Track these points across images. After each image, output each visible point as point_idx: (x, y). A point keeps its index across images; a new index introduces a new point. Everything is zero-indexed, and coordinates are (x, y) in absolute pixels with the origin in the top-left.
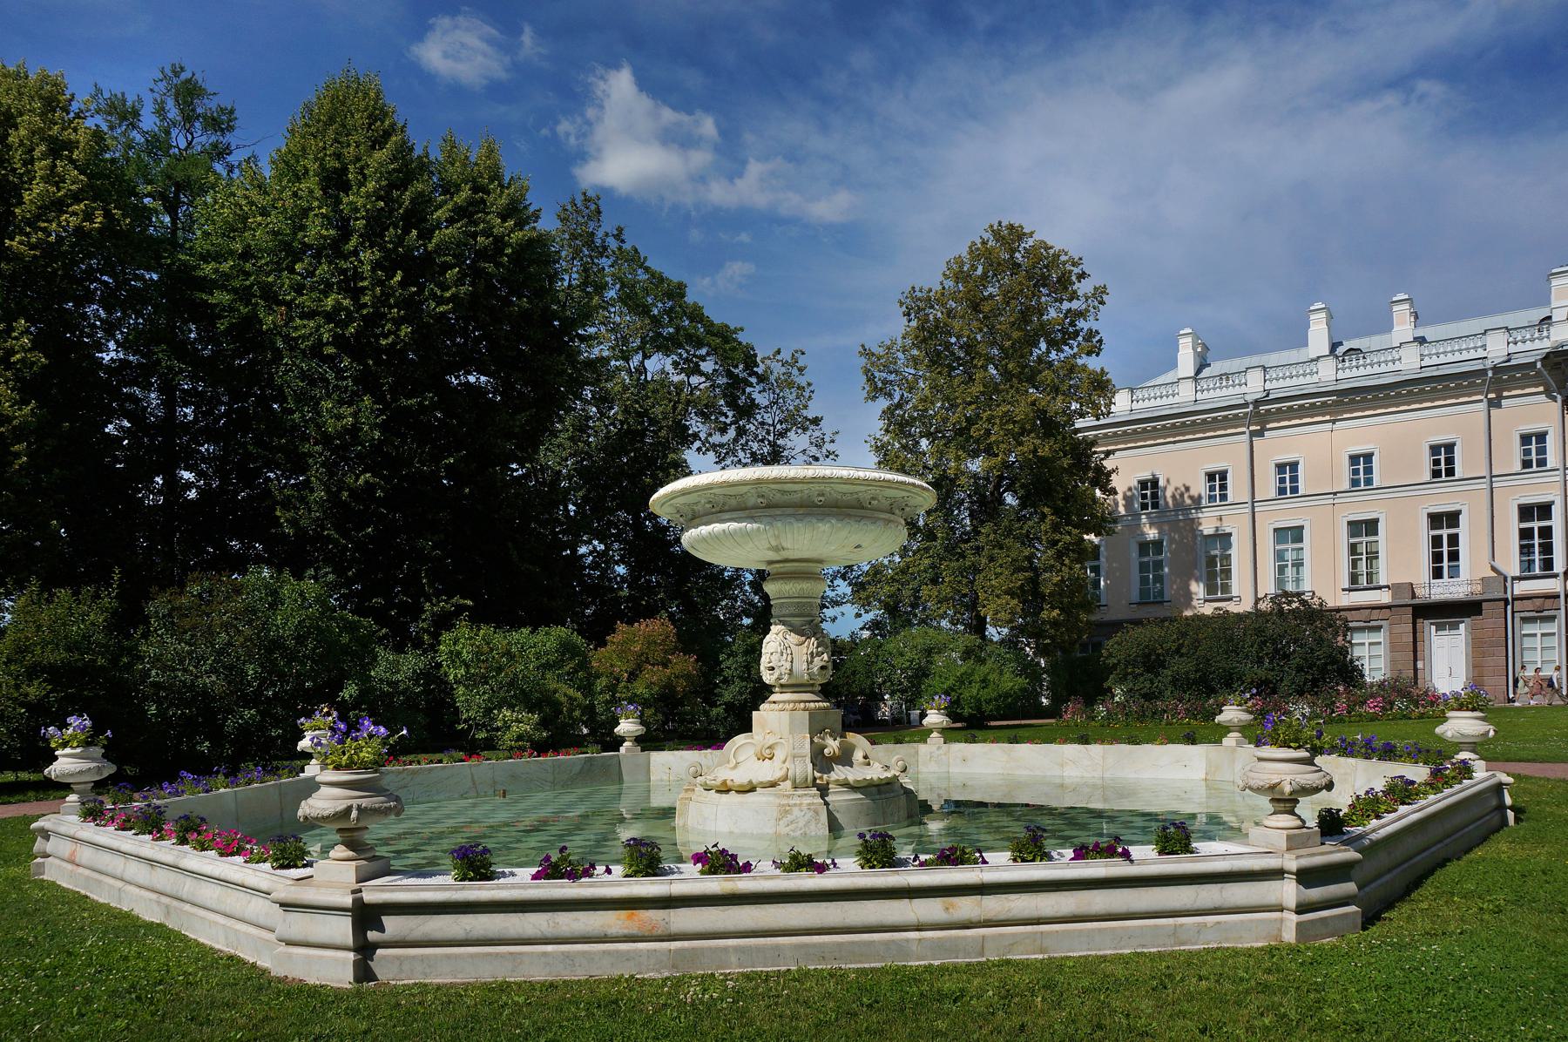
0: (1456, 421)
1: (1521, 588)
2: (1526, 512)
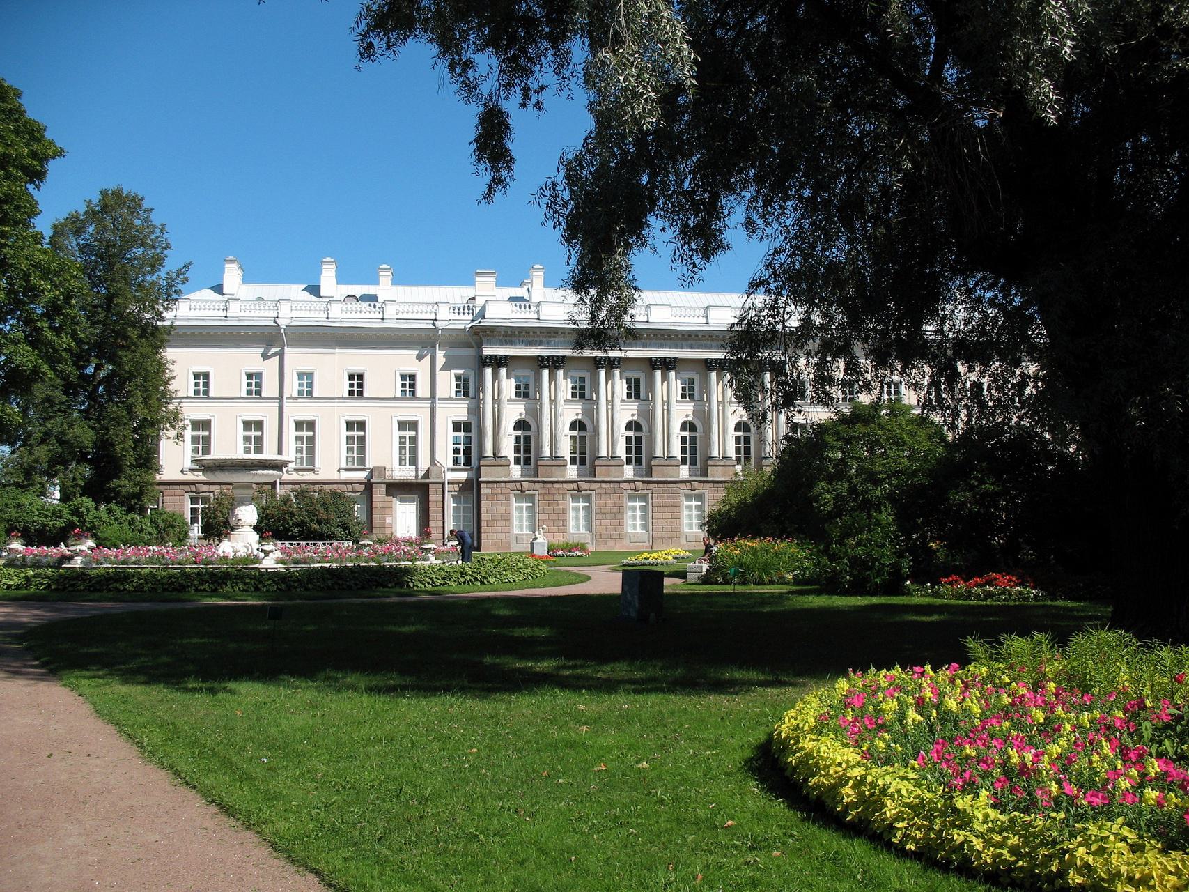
0: (406, 360)
1: (451, 476)
2: (300, 425)
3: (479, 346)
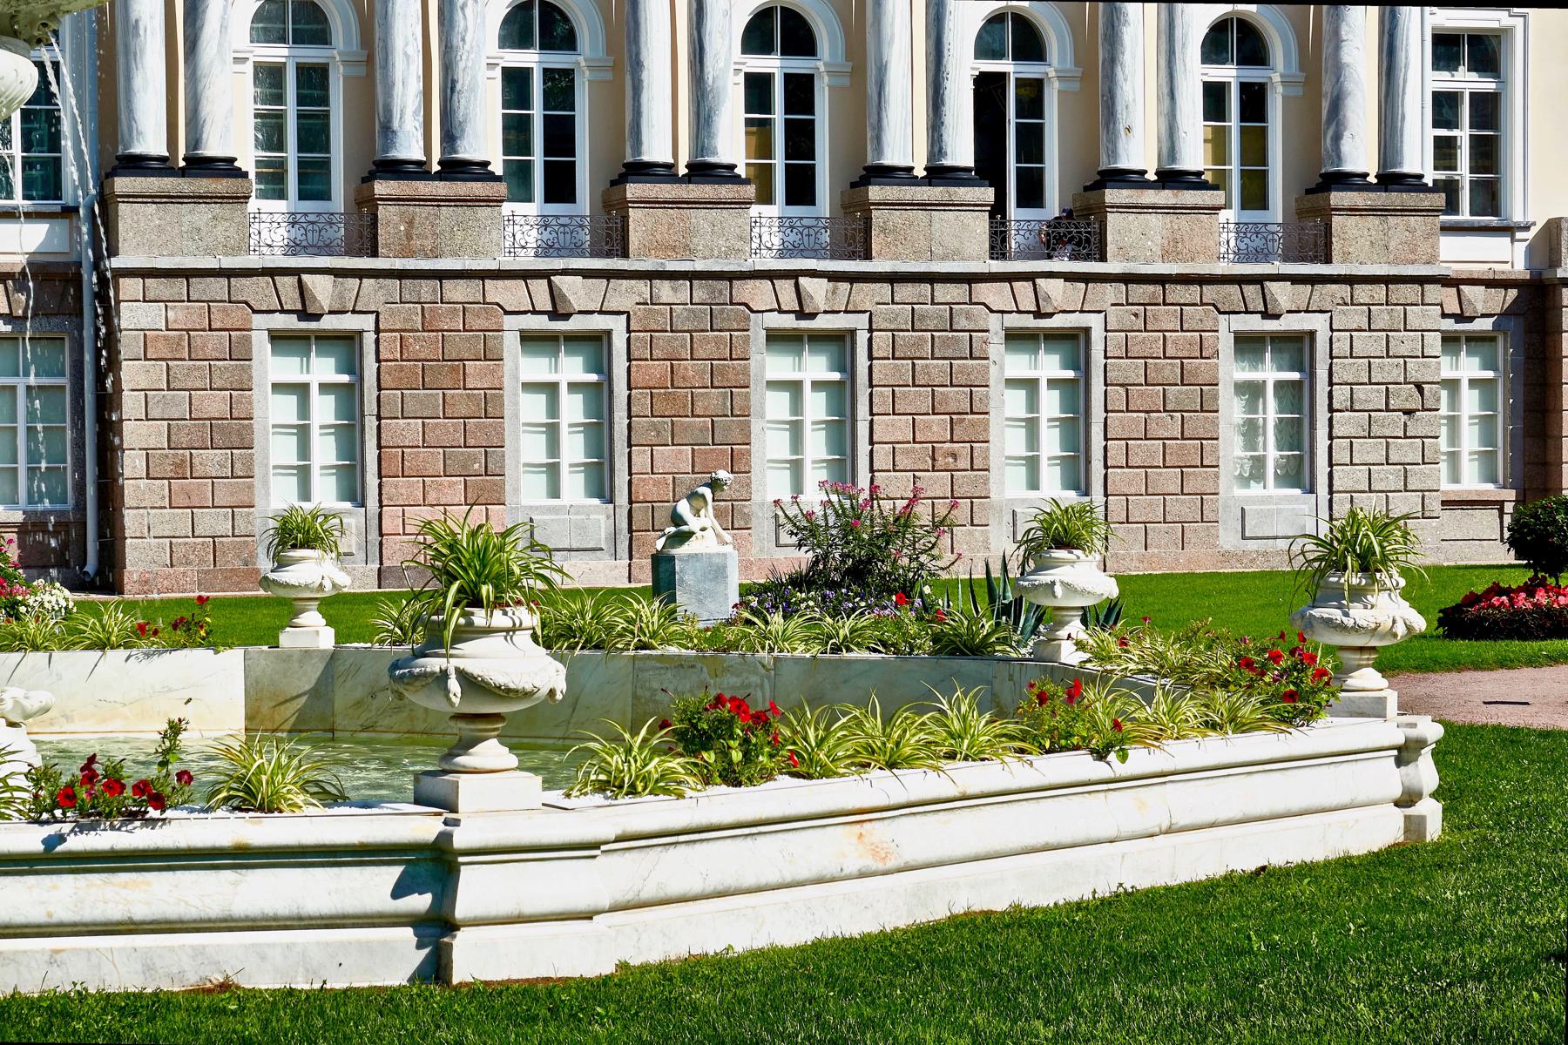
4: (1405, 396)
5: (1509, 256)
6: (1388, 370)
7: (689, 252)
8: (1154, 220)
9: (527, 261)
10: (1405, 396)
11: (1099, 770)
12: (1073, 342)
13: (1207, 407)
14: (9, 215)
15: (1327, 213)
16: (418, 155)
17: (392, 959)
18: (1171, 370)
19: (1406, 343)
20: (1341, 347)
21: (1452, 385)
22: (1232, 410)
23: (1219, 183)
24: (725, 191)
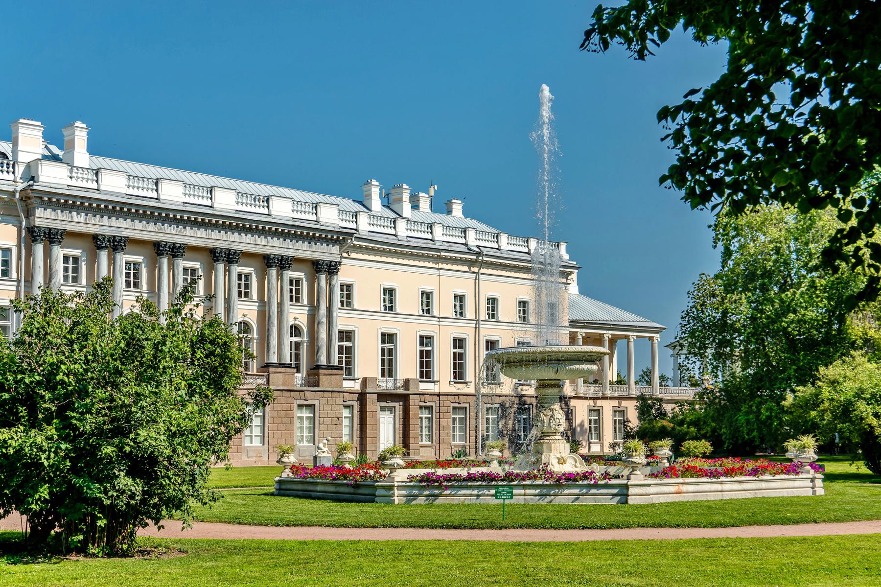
3: (29, 214)
4: (335, 421)
5: (357, 386)
6: (332, 414)
7: (341, 387)
8: (281, 376)
9: (298, 387)
10: (335, 421)
11: (771, 478)
12: (312, 407)
13: (292, 423)
14: (875, 399)
15: (318, 375)
16: (288, 362)
17: (810, 492)
18: (283, 413)
19: (335, 408)
20: (321, 408)
21: (301, 418)
22: (297, 424)
23: (341, 369)
24: (289, 370)
